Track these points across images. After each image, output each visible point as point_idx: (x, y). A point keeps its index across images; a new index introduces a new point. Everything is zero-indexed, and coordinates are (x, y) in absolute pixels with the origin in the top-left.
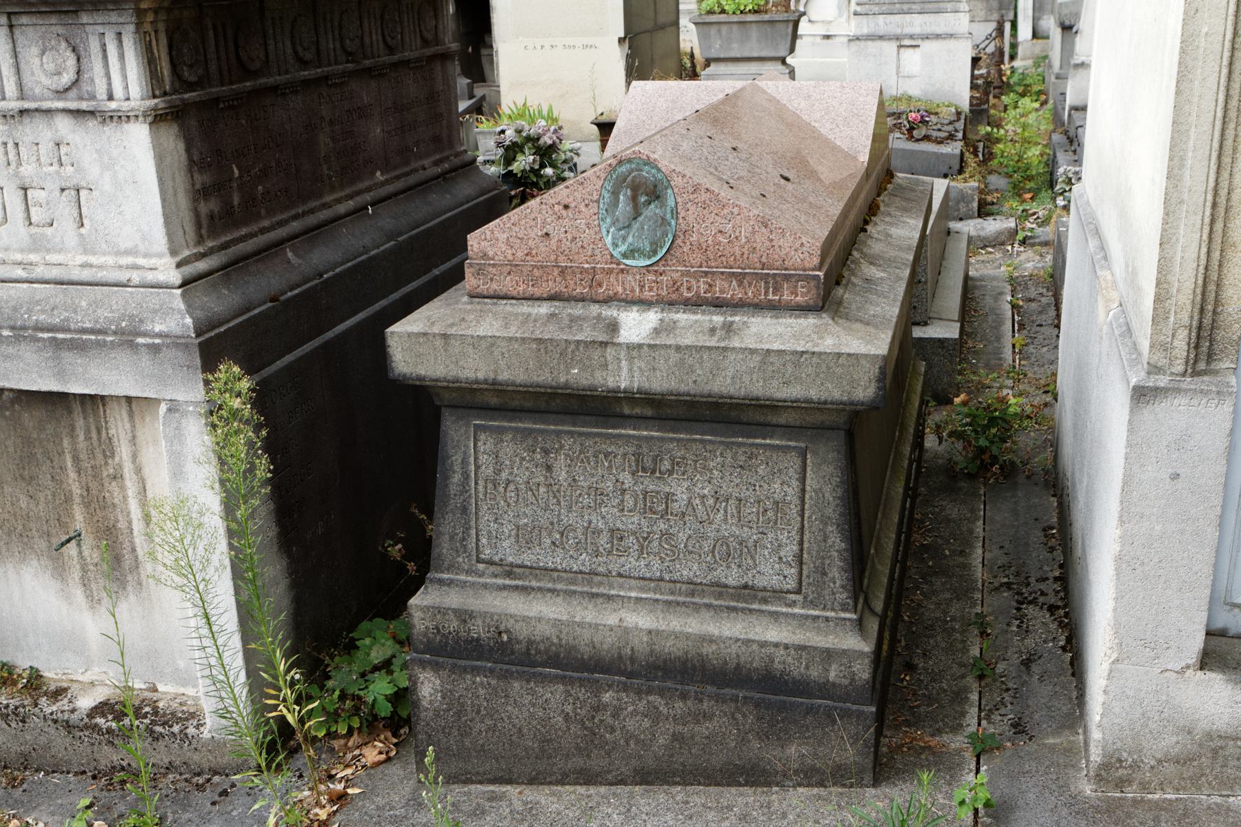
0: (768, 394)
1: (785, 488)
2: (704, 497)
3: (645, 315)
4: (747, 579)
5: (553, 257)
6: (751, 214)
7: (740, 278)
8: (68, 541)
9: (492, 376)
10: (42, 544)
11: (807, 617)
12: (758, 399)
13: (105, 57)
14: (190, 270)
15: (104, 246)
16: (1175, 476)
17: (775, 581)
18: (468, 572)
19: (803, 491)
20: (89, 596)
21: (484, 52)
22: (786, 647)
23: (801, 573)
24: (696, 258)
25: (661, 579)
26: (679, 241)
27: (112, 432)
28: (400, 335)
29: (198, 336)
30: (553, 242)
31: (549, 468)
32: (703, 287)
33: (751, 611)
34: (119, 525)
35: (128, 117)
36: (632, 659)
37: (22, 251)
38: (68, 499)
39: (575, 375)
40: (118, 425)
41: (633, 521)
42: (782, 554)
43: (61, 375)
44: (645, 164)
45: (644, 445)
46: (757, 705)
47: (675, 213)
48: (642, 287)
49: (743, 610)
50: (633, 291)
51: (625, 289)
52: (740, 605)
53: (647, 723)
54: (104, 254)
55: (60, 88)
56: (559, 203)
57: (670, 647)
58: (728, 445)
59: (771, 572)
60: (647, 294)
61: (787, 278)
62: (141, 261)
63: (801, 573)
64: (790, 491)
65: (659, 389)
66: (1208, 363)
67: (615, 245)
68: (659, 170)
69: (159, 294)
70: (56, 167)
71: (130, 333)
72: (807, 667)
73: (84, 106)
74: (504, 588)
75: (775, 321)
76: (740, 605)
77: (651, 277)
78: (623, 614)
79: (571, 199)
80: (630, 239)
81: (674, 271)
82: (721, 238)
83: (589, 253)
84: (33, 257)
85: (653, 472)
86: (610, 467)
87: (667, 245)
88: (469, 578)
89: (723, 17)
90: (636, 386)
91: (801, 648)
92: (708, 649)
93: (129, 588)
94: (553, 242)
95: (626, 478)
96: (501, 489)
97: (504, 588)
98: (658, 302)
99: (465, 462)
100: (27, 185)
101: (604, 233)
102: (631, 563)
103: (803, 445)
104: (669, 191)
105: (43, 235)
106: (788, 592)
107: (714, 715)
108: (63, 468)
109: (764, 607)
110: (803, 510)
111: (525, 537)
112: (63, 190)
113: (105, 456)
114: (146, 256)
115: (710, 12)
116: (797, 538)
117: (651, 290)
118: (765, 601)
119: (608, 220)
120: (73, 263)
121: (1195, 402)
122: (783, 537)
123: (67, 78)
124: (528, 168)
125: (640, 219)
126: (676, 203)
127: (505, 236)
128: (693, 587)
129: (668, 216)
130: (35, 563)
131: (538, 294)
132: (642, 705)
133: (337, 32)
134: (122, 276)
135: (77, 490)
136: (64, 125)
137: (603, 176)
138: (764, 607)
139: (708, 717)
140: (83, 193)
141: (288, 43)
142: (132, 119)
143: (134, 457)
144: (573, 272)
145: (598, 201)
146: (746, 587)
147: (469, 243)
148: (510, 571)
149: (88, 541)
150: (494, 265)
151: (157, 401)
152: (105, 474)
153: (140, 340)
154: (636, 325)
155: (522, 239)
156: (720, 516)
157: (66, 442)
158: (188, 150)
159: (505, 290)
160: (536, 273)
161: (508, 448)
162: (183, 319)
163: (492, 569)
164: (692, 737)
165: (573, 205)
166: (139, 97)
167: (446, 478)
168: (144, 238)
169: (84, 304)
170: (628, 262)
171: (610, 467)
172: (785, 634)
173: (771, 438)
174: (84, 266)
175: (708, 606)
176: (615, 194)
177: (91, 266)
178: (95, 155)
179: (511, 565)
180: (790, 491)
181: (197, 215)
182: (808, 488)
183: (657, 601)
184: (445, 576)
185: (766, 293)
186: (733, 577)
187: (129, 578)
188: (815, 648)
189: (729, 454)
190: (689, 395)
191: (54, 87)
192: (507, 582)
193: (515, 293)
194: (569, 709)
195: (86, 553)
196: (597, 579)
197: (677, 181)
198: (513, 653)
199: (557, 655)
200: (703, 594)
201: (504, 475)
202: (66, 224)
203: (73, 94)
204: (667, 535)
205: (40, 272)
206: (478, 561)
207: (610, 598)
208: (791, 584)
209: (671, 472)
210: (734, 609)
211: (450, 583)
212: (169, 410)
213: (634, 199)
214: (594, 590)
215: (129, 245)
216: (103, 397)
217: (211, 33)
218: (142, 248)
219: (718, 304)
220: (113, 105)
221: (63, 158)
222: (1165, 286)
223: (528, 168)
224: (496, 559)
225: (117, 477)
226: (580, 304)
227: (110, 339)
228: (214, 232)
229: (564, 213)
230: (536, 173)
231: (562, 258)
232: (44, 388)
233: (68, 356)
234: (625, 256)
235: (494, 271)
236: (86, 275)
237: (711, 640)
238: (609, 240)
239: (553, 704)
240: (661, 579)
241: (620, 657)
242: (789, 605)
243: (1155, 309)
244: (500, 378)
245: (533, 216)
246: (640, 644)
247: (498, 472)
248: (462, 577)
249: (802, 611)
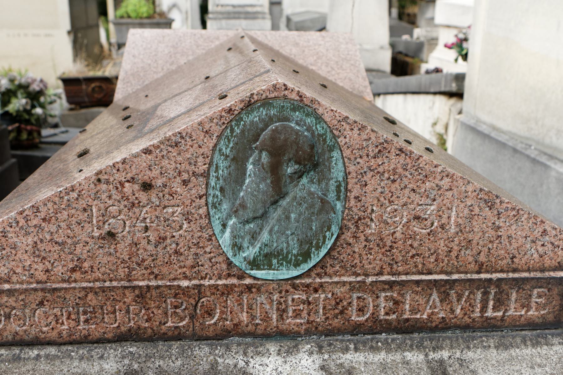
3: (292, 359)
5: (122, 272)
6: (470, 188)
24: (375, 259)
26: (347, 236)
30: (123, 249)
44: (294, 110)
47: (342, 190)
48: (282, 312)
50: (266, 318)
51: (253, 317)
56: (132, 180)
60: (291, 322)
61: (518, 283)
67: (237, 247)
68: (319, 118)
75: (505, 355)
77: (299, 296)
79: (156, 172)
80: (265, 236)
82: (416, 228)
83: (189, 263)
87: (329, 244)
89: (129, 21)
98: (308, 333)
104: (336, 154)
115: (122, 17)
119: (225, 206)
124: (21, 108)
125: (284, 203)
126: (347, 174)
127: (30, 240)
129: (332, 196)
131: (97, 335)
137: (216, 130)
144: (161, 295)
145: (206, 175)
150: (10, 292)
155: (63, 243)
159: (33, 331)
165: (159, 182)
170: (259, 274)
176: (238, 161)
193: (54, 335)
197: (350, 137)
213: (275, 169)
223: (21, 108)
229: (143, 197)
230: (28, 112)
231: (138, 272)
234: (254, 264)
235: (11, 301)
238: (225, 239)
245: (83, 203)
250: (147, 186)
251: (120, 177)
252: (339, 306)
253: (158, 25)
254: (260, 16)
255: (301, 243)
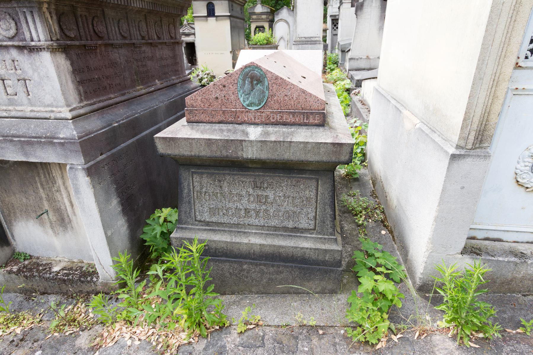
0: (306, 159)
1: (311, 193)
2: (280, 196)
3: (256, 129)
4: (296, 225)
5: (220, 107)
7: (293, 114)
8: (43, 214)
9: (197, 154)
10: (34, 215)
11: (318, 238)
12: (302, 161)
13: (27, 22)
14: (75, 113)
15: (39, 103)
16: (463, 188)
17: (306, 226)
18: (192, 225)
19: (317, 194)
20: (55, 232)
21: (194, 58)
22: (311, 249)
23: (316, 223)
24: (276, 106)
25: (264, 226)
26: (269, 99)
27: (54, 175)
28: (160, 138)
29: (79, 139)
31: (221, 187)
32: (279, 117)
33: (297, 236)
34: (62, 208)
35: (41, 49)
36: (254, 254)
37: (6, 105)
38: (41, 199)
39: (230, 153)
40: (56, 173)
41: (253, 206)
42: (309, 216)
43: (26, 155)
45: (257, 178)
46: (299, 268)
47: (268, 88)
49: (294, 236)
50: (251, 119)
52: (293, 234)
53: (259, 275)
54: (39, 106)
55: (10, 36)
57: (267, 249)
58: (289, 178)
59: (304, 223)
60: (257, 121)
61: (312, 113)
62: (54, 109)
63: (316, 223)
64: (312, 194)
65: (264, 158)
66: (480, 144)
67: (244, 101)
68: (261, 70)
69: (62, 122)
70: (14, 71)
71: (51, 138)
72: (318, 256)
73: (21, 44)
74: (205, 230)
76: (293, 234)
77: (259, 114)
78: (250, 238)
79: (226, 83)
80: (250, 99)
81: (268, 111)
84: (10, 108)
85: (260, 188)
86: (244, 187)
87: (265, 101)
88: (193, 227)
90: (255, 157)
91: (315, 249)
92: (281, 250)
93: (69, 229)
94: (220, 101)
95: (251, 191)
96: (203, 195)
97: (205, 230)
99: (189, 185)
100: (3, 78)
101: (240, 96)
102: (253, 221)
103: (317, 177)
104: (266, 79)
105: (14, 99)
106: (311, 229)
107: (284, 272)
108: (37, 188)
109: (302, 235)
110: (317, 200)
111: (213, 211)
112: (19, 80)
113: (53, 183)
114: (56, 107)
116: (315, 211)
117: (258, 119)
118: (302, 233)
119: (241, 91)
120: (27, 110)
121: (475, 160)
122: (310, 210)
123: (12, 32)
127: (200, 98)
128: (276, 228)
129: (265, 89)
130: (32, 221)
131: (214, 121)
132: (258, 269)
133: (137, 28)
134: (47, 115)
135: (44, 196)
136: (14, 53)
137: (239, 73)
138: (302, 235)
139: (281, 272)
140: (27, 82)
141: (117, 29)
142: (43, 50)
143: (64, 183)
146: (295, 228)
147: (186, 101)
148: (208, 224)
149: (51, 214)
150: (196, 110)
151: (65, 165)
152: (53, 190)
153: (55, 141)
154: (254, 133)
155: (207, 99)
156: (286, 203)
157: (37, 179)
158: (72, 64)
160: (213, 112)
161: (205, 180)
162: (73, 132)
163: (201, 223)
164: (276, 279)
165: (227, 85)
166: (44, 40)
167: (182, 191)
168: (55, 100)
169: (32, 126)
171: (244, 187)
172: (310, 244)
173: (305, 174)
174: (31, 111)
175: (281, 235)
176: (244, 80)
177: (35, 111)
178: (29, 66)
179: (208, 222)
180: (312, 194)
181: (79, 91)
182: (319, 193)
183: (262, 233)
184: (184, 226)
185: (304, 120)
186: (290, 225)
187: (68, 226)
188: (321, 249)
189: (289, 181)
190: (275, 160)
191: (7, 36)
192: (207, 228)
193: (205, 121)
194: (231, 271)
195: (51, 218)
196: (240, 226)
197: (269, 75)
198: (210, 252)
199: (226, 253)
200: (279, 231)
201: (204, 190)
202: (22, 95)
203: (16, 38)
204: (266, 211)
205: (13, 114)
206: (196, 220)
207: (245, 233)
208: (312, 227)
209: (267, 188)
210: (291, 236)
211: (186, 228)
212: (70, 168)
213: (252, 82)
214: (239, 230)
215: (49, 103)
216: (49, 164)
217: (80, 19)
218: (54, 104)
219: (285, 124)
220: (33, 44)
221: (17, 67)
222: (468, 114)
224: (202, 220)
225: (58, 191)
226: (231, 125)
227: (43, 140)
228: (87, 98)
229: (224, 89)
232: (20, 160)
233: (27, 148)
234: (248, 105)
236: (32, 115)
237: (283, 247)
238: (241, 99)
239: (225, 269)
240: (264, 226)
241: (249, 253)
242: (310, 234)
243: (463, 124)
244: (201, 154)
246: (257, 249)
247: (201, 189)
248: (190, 226)
249: (316, 236)
250: (224, 86)
251: (219, 84)
252: (268, 117)
253: (271, 48)
254: (318, 42)
255: (258, 101)
